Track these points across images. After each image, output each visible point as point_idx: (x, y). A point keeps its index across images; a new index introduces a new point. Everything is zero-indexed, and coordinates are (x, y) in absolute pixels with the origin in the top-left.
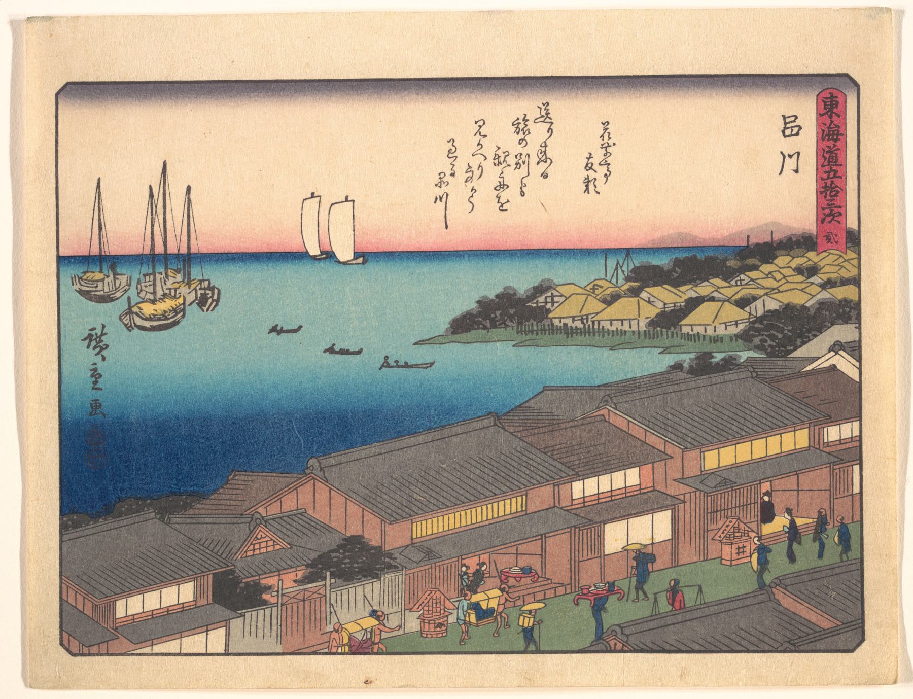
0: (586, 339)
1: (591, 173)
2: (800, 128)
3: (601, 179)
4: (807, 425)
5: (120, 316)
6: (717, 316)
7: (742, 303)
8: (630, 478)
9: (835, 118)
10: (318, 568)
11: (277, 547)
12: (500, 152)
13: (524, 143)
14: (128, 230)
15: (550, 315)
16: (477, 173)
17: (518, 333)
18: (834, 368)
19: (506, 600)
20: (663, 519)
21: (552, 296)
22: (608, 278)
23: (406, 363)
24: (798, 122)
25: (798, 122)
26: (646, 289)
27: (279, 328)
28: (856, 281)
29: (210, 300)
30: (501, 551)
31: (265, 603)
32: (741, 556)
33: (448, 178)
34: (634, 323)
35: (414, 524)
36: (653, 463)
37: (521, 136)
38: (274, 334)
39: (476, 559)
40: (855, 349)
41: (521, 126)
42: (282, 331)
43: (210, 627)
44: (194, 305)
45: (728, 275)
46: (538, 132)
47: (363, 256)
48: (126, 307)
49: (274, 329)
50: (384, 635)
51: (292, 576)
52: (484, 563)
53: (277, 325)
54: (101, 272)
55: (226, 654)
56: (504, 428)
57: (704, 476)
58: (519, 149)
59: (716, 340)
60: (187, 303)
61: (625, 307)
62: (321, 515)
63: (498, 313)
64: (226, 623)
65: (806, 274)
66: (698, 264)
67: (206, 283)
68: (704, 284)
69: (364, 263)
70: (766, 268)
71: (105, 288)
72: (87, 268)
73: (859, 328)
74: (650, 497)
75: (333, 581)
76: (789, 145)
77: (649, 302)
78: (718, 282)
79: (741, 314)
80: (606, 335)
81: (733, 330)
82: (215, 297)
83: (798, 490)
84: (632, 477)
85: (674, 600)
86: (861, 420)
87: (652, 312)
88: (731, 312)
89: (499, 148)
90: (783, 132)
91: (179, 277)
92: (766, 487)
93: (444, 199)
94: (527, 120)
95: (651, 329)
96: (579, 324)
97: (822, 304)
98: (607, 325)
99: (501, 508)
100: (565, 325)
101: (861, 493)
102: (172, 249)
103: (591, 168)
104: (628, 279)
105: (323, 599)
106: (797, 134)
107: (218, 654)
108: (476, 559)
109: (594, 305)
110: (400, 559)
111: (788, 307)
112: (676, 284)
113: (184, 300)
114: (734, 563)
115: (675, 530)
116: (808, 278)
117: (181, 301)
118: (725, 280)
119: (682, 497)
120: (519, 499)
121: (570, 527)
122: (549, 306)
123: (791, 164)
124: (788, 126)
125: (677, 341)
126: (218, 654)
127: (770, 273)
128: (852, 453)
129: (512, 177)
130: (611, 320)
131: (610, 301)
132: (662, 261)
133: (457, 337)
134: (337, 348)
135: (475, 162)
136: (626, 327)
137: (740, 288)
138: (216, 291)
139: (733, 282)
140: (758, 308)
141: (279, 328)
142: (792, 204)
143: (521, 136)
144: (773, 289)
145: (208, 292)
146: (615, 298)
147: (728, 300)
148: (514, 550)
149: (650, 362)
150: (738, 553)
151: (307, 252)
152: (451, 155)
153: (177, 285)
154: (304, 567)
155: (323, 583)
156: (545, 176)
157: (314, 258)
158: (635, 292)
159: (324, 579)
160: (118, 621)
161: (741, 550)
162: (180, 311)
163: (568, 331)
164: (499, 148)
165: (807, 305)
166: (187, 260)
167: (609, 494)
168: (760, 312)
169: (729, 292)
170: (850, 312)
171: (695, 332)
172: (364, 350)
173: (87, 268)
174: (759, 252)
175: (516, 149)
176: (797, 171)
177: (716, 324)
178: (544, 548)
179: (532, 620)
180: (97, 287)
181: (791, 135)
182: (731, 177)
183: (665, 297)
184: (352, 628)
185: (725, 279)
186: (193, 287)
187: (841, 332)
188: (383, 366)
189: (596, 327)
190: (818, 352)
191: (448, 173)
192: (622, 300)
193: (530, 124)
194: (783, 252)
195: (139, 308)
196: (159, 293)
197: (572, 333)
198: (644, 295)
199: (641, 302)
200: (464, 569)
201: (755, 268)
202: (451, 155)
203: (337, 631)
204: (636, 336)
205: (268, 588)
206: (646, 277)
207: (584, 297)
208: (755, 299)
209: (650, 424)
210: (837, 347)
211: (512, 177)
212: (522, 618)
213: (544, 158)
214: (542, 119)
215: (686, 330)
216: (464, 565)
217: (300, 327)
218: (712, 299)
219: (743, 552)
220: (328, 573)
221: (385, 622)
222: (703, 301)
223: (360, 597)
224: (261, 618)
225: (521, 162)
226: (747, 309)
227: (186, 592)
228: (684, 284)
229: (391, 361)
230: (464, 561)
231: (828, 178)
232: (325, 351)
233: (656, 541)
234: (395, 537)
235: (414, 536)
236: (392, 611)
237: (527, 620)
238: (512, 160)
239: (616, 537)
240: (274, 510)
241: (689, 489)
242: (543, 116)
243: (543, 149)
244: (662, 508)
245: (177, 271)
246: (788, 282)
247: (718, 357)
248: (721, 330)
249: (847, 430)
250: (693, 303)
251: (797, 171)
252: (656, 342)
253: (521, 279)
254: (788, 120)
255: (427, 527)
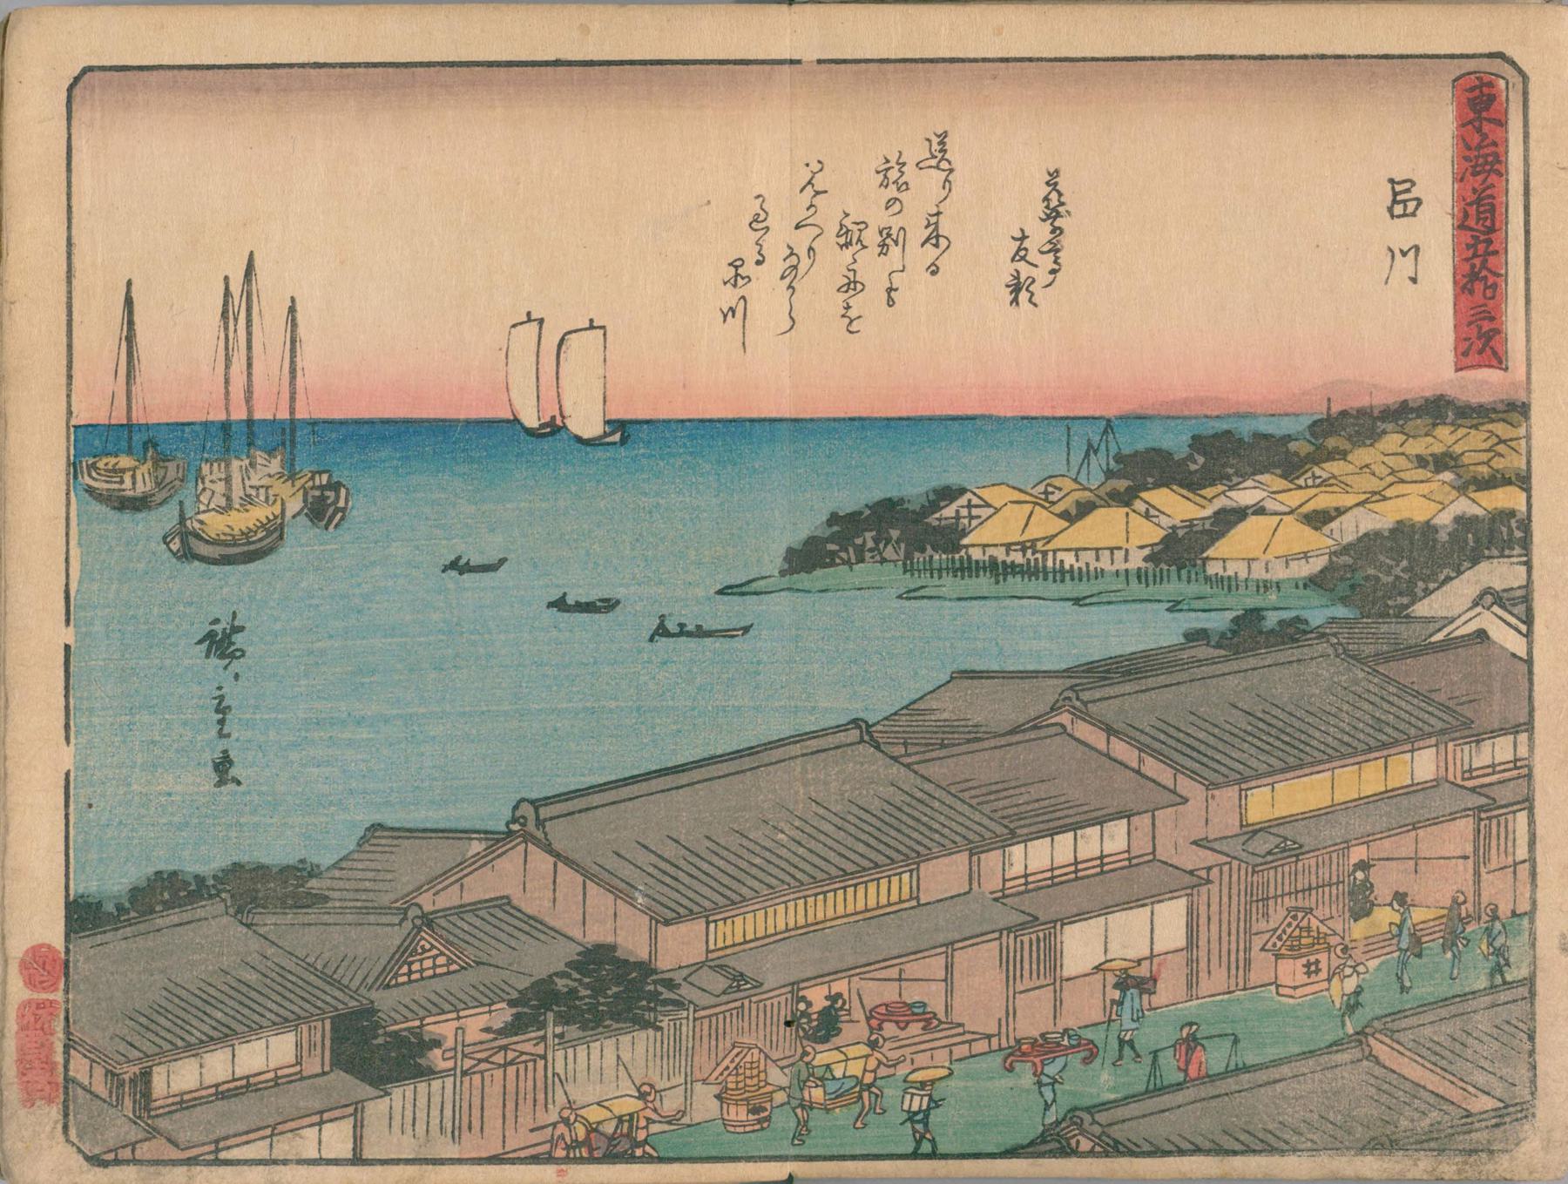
0: (1035, 586)
1: (1022, 266)
2: (1419, 202)
3: (1042, 276)
5: (165, 538)
7: (1319, 519)
9: (1486, 127)
10: (539, 1005)
12: (847, 222)
13: (897, 207)
14: (183, 374)
16: (805, 262)
19: (880, 1063)
20: (1171, 920)
21: (969, 506)
22: (1073, 474)
23: (699, 627)
24: (1415, 193)
25: (1415, 193)
26: (1143, 495)
27: (462, 562)
28: (1523, 481)
29: (331, 510)
30: (877, 975)
32: (1314, 978)
33: (749, 269)
34: (1119, 555)
35: (712, 926)
36: (1129, 817)
37: (892, 191)
38: (454, 573)
39: (824, 990)
40: (1519, 605)
41: (893, 175)
42: (468, 568)
43: (326, 1116)
44: (302, 519)
45: (1291, 467)
47: (622, 429)
48: (175, 521)
49: (454, 565)
50: (654, 1128)
51: (483, 1021)
52: (839, 995)
53: (459, 558)
56: (878, 748)
59: (1265, 586)
60: (289, 514)
61: (1105, 526)
62: (535, 902)
63: (869, 535)
67: (325, 477)
68: (1249, 483)
69: (623, 441)
70: (1362, 455)
71: (143, 484)
73: (1528, 565)
74: (456, 1136)
76: (1401, 233)
77: (1147, 516)
78: (1273, 481)
80: (1068, 577)
81: (1304, 570)
82: (341, 504)
83: (1416, 859)
85: (1187, 1063)
87: (1152, 534)
89: (847, 215)
90: (1390, 210)
91: (275, 465)
92: (1358, 853)
93: (739, 313)
94: (904, 164)
95: (1150, 565)
96: (1017, 557)
97: (1464, 523)
98: (1069, 559)
99: (770, 921)
100: (993, 560)
103: (1023, 258)
104: (1109, 474)
105: (541, 1063)
106: (1413, 214)
108: (824, 990)
109: (1044, 524)
110: (685, 991)
111: (1402, 529)
117: (277, 510)
118: (1284, 477)
119: (1203, 874)
120: (906, 877)
121: (1001, 931)
123: (1405, 265)
126: (336, 1162)
129: (873, 269)
132: (1176, 442)
133: (803, 580)
134: (570, 601)
136: (1105, 563)
137: (1313, 491)
138: (343, 492)
139: (1301, 482)
140: (1350, 528)
141: (462, 562)
142: (1404, 336)
143: (892, 191)
144: (1375, 493)
145: (328, 493)
146: (1085, 509)
148: (894, 973)
150: (1317, 962)
151: (516, 420)
153: (266, 481)
154: (504, 1005)
156: (934, 270)
157: (530, 432)
158: (1125, 499)
159: (542, 1026)
162: (275, 531)
163: (1000, 570)
164: (847, 215)
165: (1436, 521)
167: (1022, 881)
168: (1350, 537)
171: (1230, 572)
172: (438, 571)
174: (1345, 427)
175: (878, 218)
176: (1414, 280)
177: (1269, 556)
178: (949, 968)
179: (926, 1099)
181: (1404, 215)
183: (1176, 507)
187: (1500, 573)
188: (656, 633)
189: (1050, 563)
190: (1451, 602)
191: (751, 256)
192: (1100, 513)
193: (910, 172)
194: (1390, 426)
196: (237, 492)
198: (1139, 506)
199: (1132, 515)
200: (802, 1006)
201: (1343, 455)
204: (1122, 578)
205: (437, 1043)
206: (1139, 472)
208: (1340, 512)
210: (1491, 598)
211: (873, 269)
212: (908, 1097)
214: (933, 162)
215: (1213, 569)
216: (803, 999)
217: (502, 561)
218: (1260, 511)
220: (550, 1016)
221: (658, 1104)
223: (610, 1058)
224: (422, 1102)
225: (888, 241)
226: (1326, 530)
229: (671, 626)
231: (1475, 256)
232: (551, 605)
233: (1158, 949)
234: (679, 947)
236: (668, 1085)
237: (917, 1099)
238: (871, 237)
239: (1081, 947)
244: (1172, 893)
245: (271, 453)
246: (1403, 481)
247: (1272, 619)
248: (1280, 573)
249: (1501, 750)
250: (1229, 518)
251: (1414, 280)
254: (1398, 188)
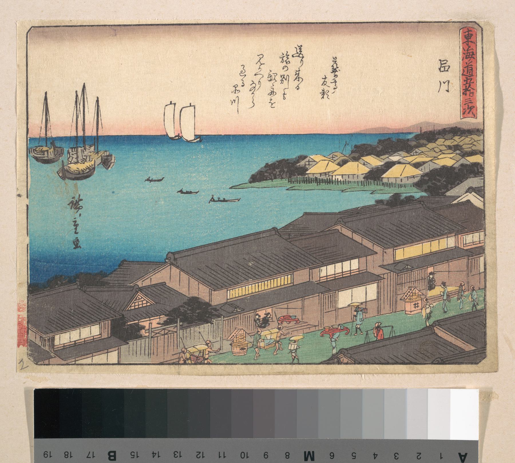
2: (449, 67)
4: (454, 234)
6: (403, 171)
7: (417, 165)
8: (353, 265)
11: (148, 304)
12: (271, 73)
13: (286, 68)
15: (307, 172)
16: (258, 86)
17: (289, 182)
18: (468, 201)
19: (281, 334)
20: (372, 290)
21: (309, 161)
23: (224, 199)
28: (482, 153)
31: (141, 337)
32: (417, 308)
35: (229, 291)
39: (264, 312)
40: (480, 191)
46: (295, 62)
47: (201, 138)
48: (61, 166)
49: (148, 180)
52: (269, 313)
54: (46, 146)
55: (119, 364)
57: (396, 263)
58: (283, 72)
64: (118, 346)
65: (453, 149)
66: (392, 143)
70: (431, 145)
72: (44, 149)
75: (181, 323)
76: (445, 77)
78: (403, 154)
79: (418, 172)
80: (339, 183)
83: (449, 271)
84: (355, 264)
86: (485, 231)
88: (411, 171)
90: (440, 69)
98: (340, 178)
100: (316, 178)
101: (485, 272)
102: (88, 133)
107: (113, 364)
108: (264, 312)
112: (378, 154)
113: (95, 162)
114: (413, 313)
115: (378, 293)
116: (454, 151)
122: (307, 166)
124: (443, 66)
125: (379, 187)
126: (113, 364)
127: (433, 149)
128: (479, 251)
129: (279, 87)
130: (342, 175)
131: (342, 163)
132: (374, 142)
135: (256, 79)
139: (412, 154)
144: (435, 157)
147: (409, 163)
149: (364, 199)
152: (241, 74)
155: (176, 325)
158: (356, 159)
159: (177, 323)
160: (55, 347)
161: (416, 305)
166: (97, 140)
169: (409, 159)
170: (477, 170)
173: (44, 149)
174: (429, 136)
179: (296, 346)
180: (44, 155)
182: (405, 89)
183: (374, 162)
184: (192, 350)
185: (408, 152)
186: (100, 155)
187: (473, 182)
188: (211, 200)
190: (461, 193)
195: (69, 167)
197: (320, 182)
199: (359, 164)
200: (257, 317)
201: (424, 145)
202: (241, 74)
203: (183, 352)
205: (143, 328)
207: (327, 162)
209: (366, 235)
210: (470, 190)
211: (279, 87)
212: (290, 345)
213: (298, 77)
215: (385, 181)
216: (258, 314)
218: (399, 163)
219: (418, 307)
222: (395, 164)
227: (94, 331)
228: (384, 154)
230: (257, 313)
232: (178, 192)
234: (218, 298)
235: (228, 298)
238: (278, 78)
239: (345, 298)
240: (147, 283)
241: (388, 271)
242: (297, 53)
243: (297, 73)
246: (444, 153)
250: (389, 165)
251: (448, 91)
252: (367, 188)
253: (290, 153)
255: (236, 293)
